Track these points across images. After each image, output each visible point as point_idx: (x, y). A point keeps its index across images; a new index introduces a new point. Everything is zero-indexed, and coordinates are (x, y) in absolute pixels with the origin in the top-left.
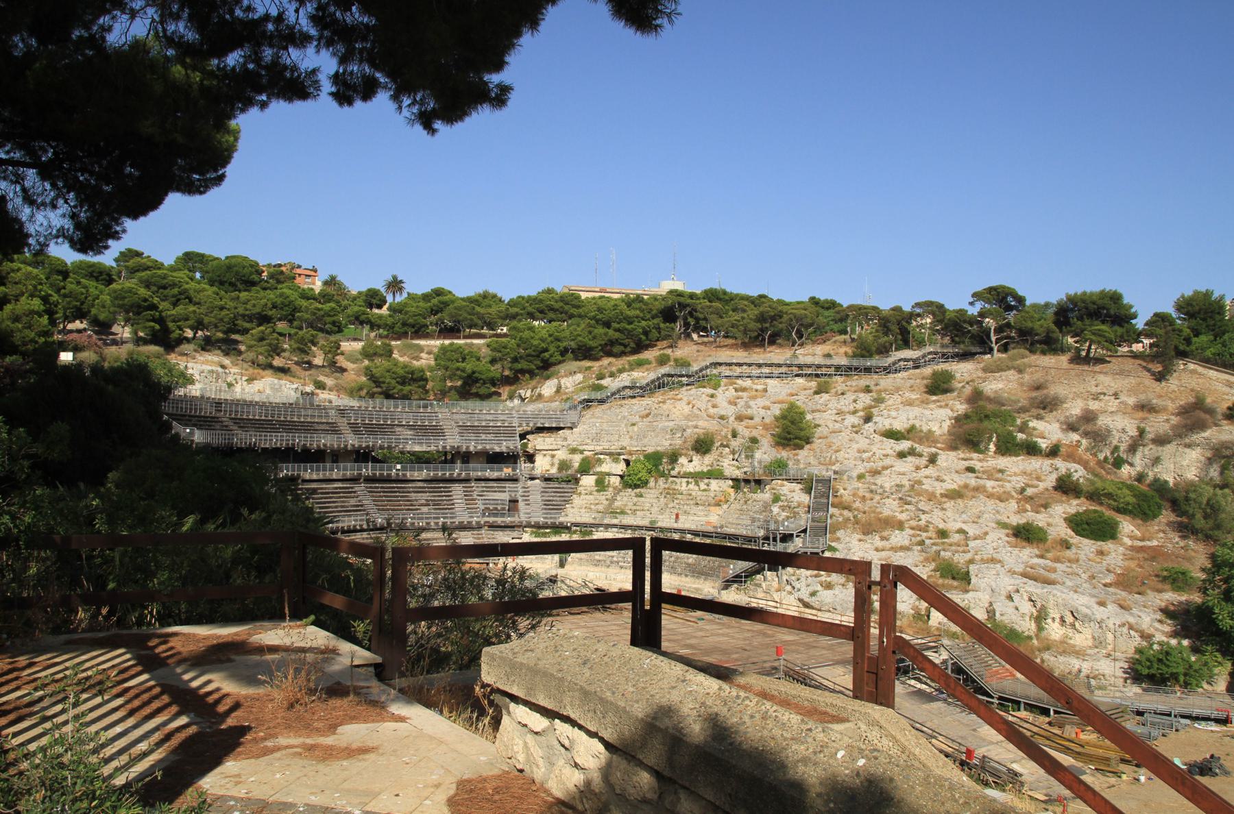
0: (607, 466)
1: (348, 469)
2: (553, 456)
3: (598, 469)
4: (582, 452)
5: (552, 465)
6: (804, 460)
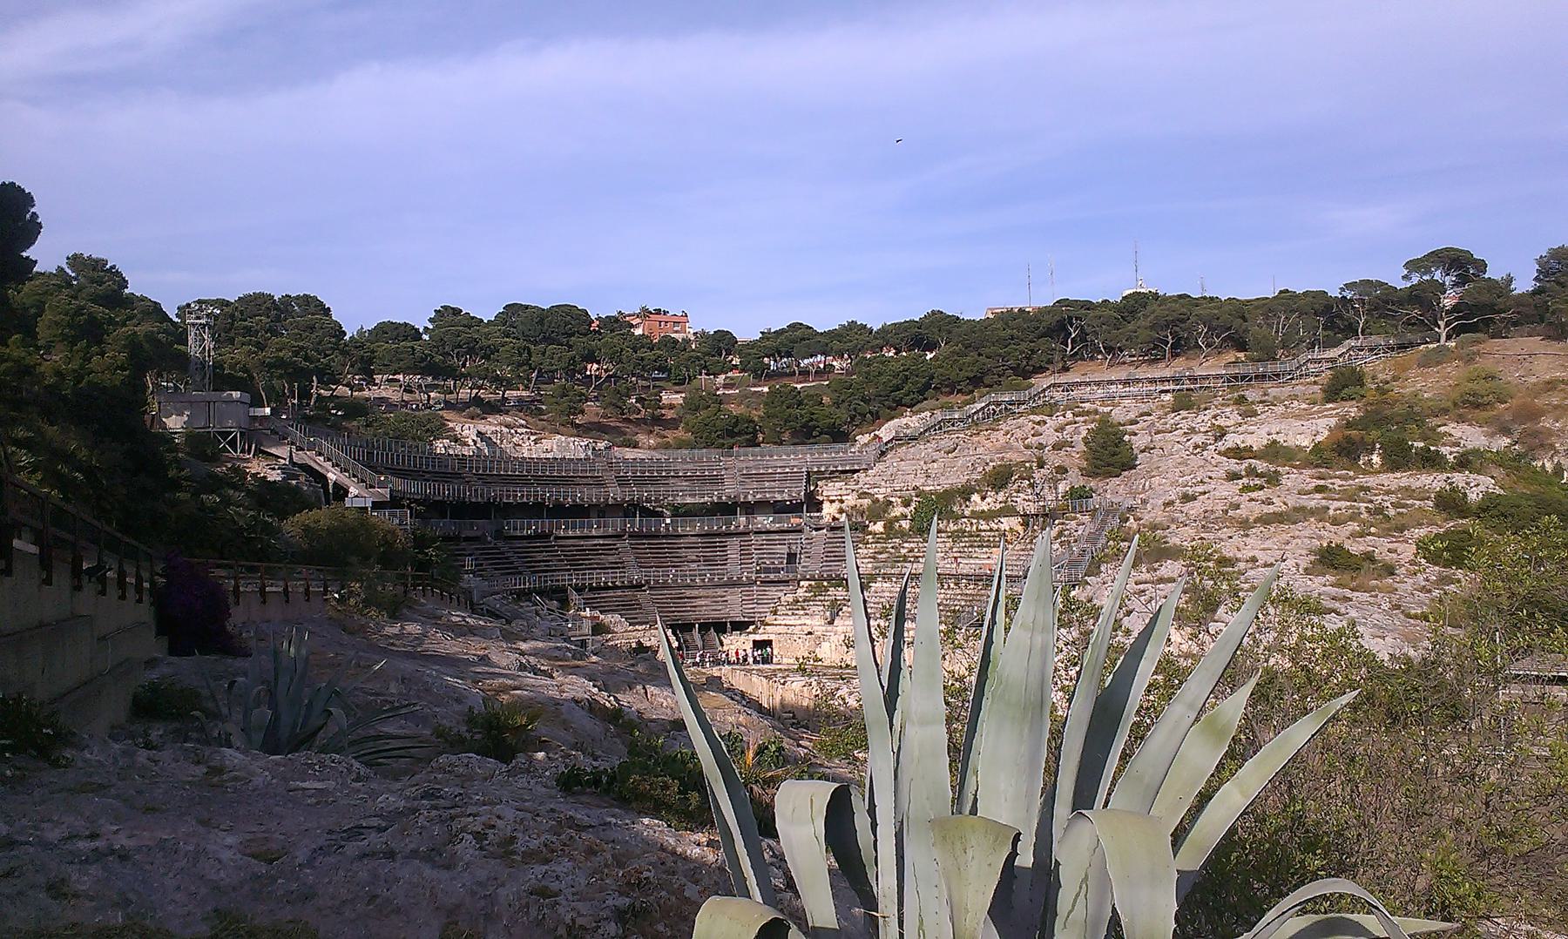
1: (615, 524)
6: (1113, 491)
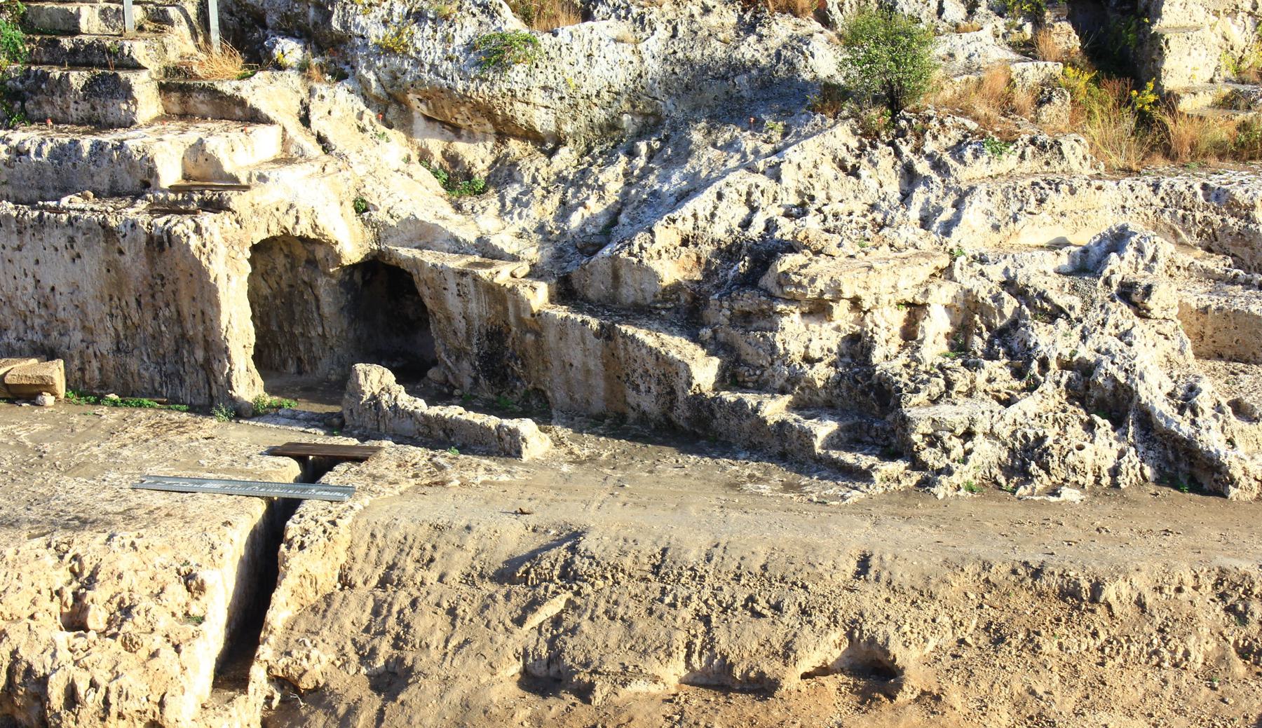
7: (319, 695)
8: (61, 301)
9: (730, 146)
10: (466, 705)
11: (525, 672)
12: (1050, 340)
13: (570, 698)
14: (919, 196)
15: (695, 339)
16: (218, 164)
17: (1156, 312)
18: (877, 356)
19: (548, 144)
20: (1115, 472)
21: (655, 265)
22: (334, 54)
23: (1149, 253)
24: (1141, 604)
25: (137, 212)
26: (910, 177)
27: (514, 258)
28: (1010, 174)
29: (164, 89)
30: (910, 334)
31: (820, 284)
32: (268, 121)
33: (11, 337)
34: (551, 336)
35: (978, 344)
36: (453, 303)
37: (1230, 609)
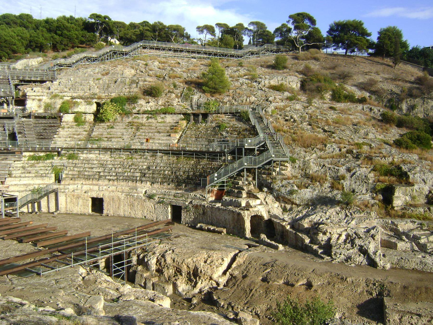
0: (82, 108)
2: (40, 100)
3: (76, 110)
4: (62, 98)
5: (39, 107)
7: (235, 277)
8: (227, 221)
9: (322, 209)
10: (252, 282)
11: (262, 278)
12: (358, 242)
13: (266, 283)
14: (347, 218)
15: (308, 236)
16: (250, 204)
17: (376, 239)
18: (332, 241)
19: (298, 206)
20: (361, 262)
21: (304, 225)
22: (271, 190)
23: (378, 230)
24: (353, 282)
25: (237, 210)
26: (346, 216)
27: (287, 221)
28: (362, 217)
29: (247, 193)
30: (338, 239)
31: (324, 230)
32: (259, 199)
33: (221, 225)
34: (289, 233)
35: (348, 241)
36: (277, 227)
37: (367, 285)
